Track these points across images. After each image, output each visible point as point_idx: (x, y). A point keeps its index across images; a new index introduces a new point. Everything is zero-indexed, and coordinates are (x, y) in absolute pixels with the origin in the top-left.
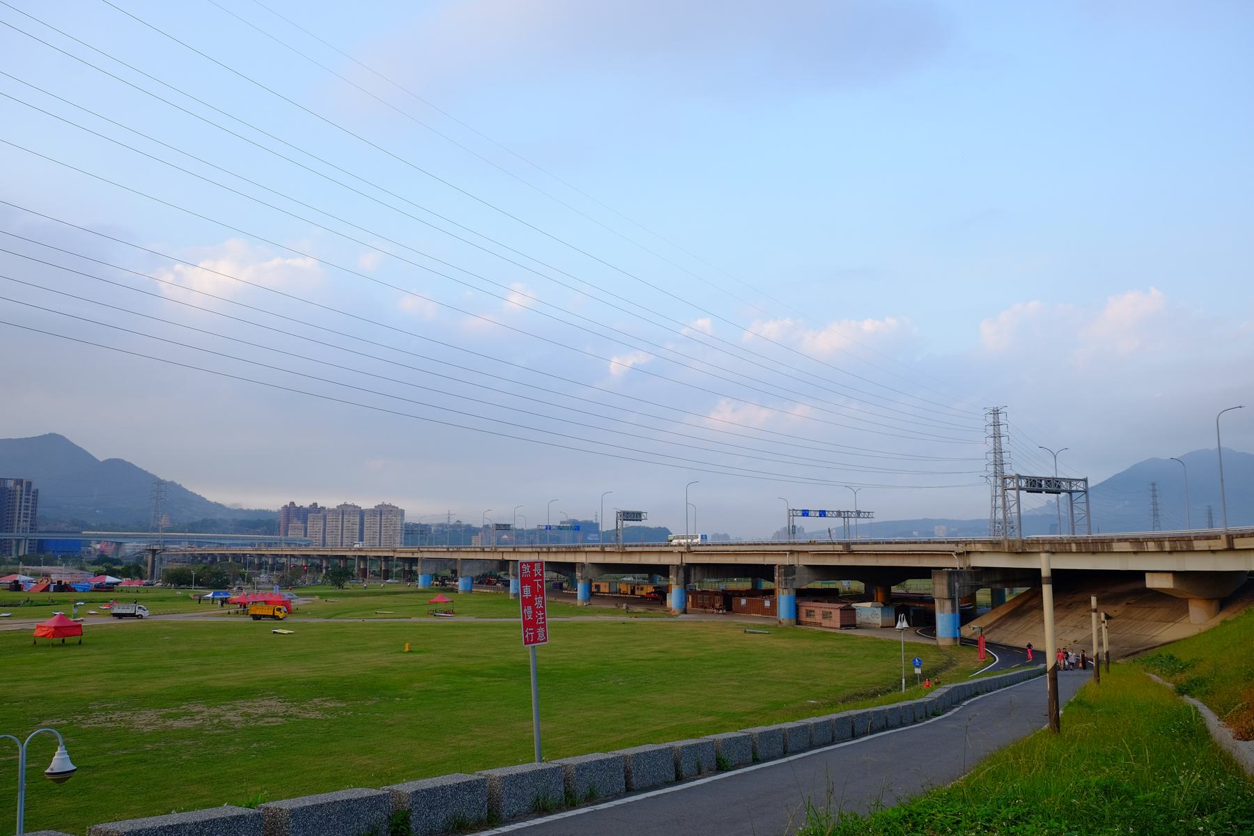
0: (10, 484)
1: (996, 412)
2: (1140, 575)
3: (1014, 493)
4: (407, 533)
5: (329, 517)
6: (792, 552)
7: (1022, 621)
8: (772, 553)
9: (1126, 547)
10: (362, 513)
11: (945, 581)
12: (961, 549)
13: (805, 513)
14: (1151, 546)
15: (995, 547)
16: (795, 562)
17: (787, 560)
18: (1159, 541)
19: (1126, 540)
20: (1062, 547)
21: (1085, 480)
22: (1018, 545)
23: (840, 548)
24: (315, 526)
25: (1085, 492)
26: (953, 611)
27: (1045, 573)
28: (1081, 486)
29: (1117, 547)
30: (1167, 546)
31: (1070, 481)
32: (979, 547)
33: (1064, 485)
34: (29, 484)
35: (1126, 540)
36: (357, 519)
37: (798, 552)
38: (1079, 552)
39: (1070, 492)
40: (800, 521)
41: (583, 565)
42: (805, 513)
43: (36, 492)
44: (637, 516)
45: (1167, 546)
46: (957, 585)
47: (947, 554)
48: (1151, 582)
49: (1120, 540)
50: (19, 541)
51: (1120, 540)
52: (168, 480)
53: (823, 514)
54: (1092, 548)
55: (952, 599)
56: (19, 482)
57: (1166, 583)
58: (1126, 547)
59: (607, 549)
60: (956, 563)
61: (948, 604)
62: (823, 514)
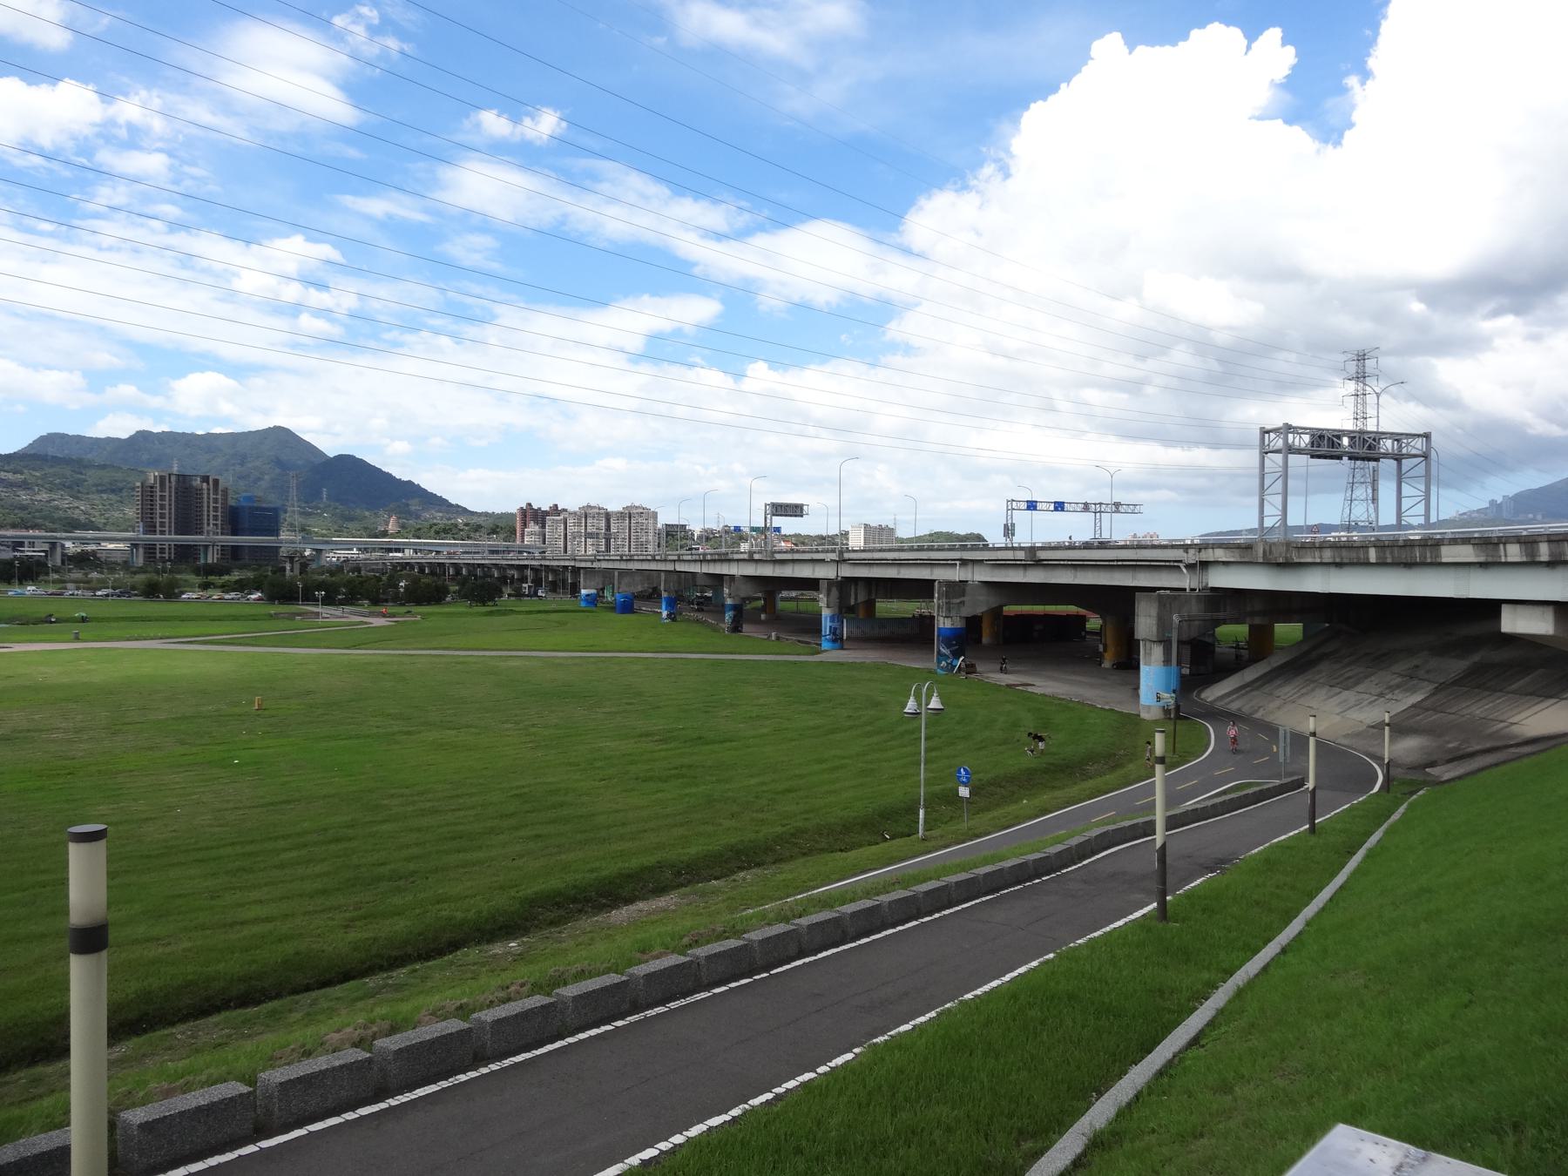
0: (197, 482)
1: (1361, 357)
2: (1491, 608)
3: (1278, 458)
4: (668, 535)
5: (570, 522)
6: (964, 562)
7: (1299, 680)
8: (932, 564)
9: (1467, 553)
10: (608, 516)
11: (1154, 611)
12: (1192, 557)
13: (1032, 506)
14: (1514, 553)
15: (1244, 551)
16: (969, 578)
17: (956, 575)
18: (1529, 542)
19: (1466, 541)
20: (1353, 555)
21: (1427, 436)
22: (1276, 552)
23: (1021, 555)
24: (554, 531)
25: (1426, 456)
26: (1167, 661)
27: (825, 645)
28: (1419, 444)
29: (1448, 554)
30: (1544, 552)
31: (1397, 437)
32: (1220, 555)
33: (1387, 445)
34: (216, 482)
35: (1466, 541)
36: (603, 524)
37: (974, 562)
38: (1381, 564)
39: (1398, 458)
40: (1022, 518)
41: (732, 577)
42: (1032, 506)
43: (225, 491)
44: (795, 510)
45: (1544, 552)
46: (1176, 618)
47: (1172, 567)
48: (1511, 623)
49: (1454, 541)
50: (206, 547)
51: (1454, 541)
52: (405, 479)
53: (1059, 506)
54: (1404, 556)
55: (1165, 642)
56: (205, 479)
57: (1539, 625)
58: (1467, 553)
59: (756, 557)
60: (1185, 581)
61: (1158, 652)
62: (1059, 506)
